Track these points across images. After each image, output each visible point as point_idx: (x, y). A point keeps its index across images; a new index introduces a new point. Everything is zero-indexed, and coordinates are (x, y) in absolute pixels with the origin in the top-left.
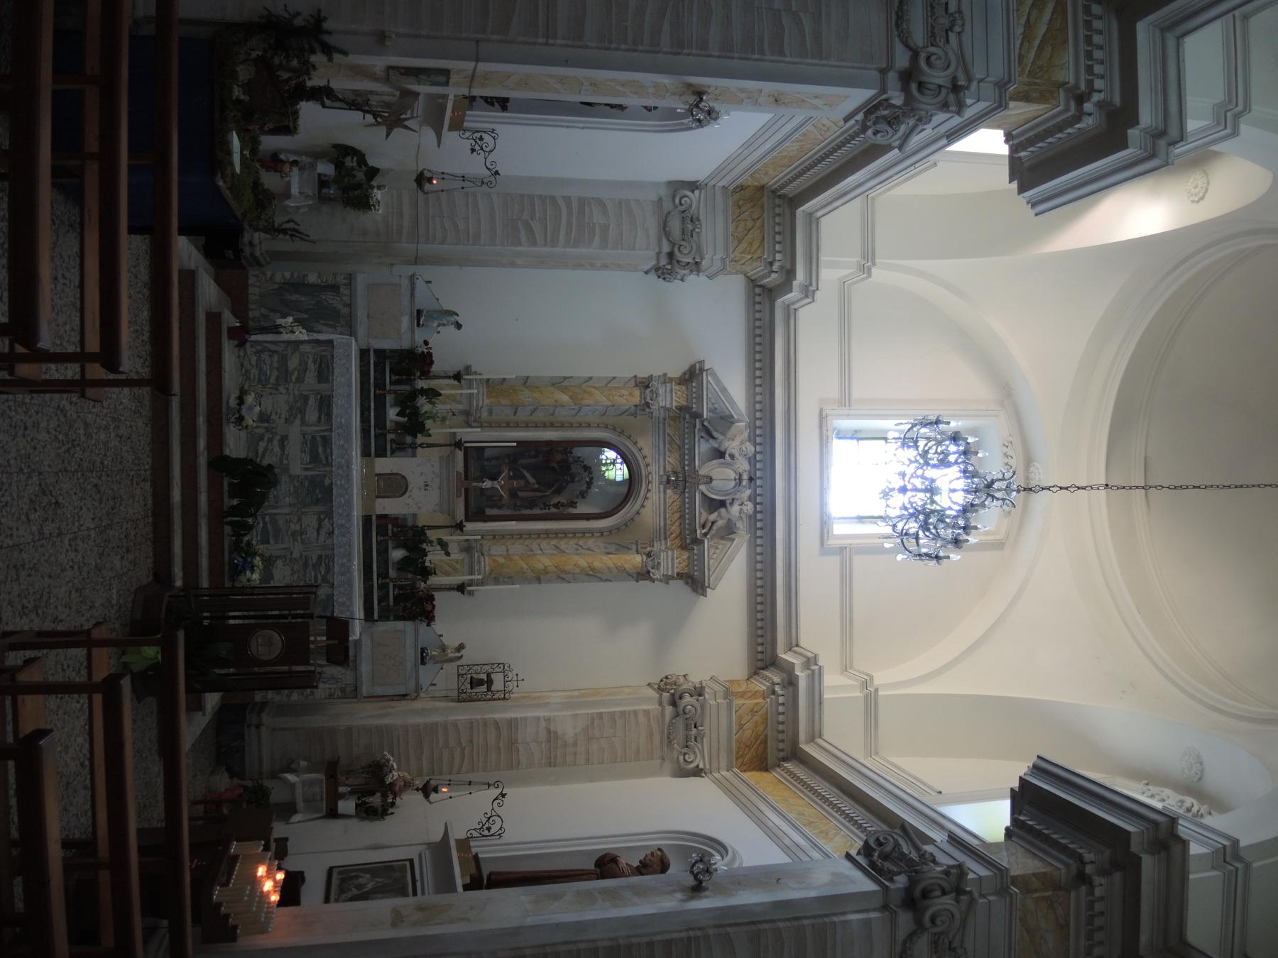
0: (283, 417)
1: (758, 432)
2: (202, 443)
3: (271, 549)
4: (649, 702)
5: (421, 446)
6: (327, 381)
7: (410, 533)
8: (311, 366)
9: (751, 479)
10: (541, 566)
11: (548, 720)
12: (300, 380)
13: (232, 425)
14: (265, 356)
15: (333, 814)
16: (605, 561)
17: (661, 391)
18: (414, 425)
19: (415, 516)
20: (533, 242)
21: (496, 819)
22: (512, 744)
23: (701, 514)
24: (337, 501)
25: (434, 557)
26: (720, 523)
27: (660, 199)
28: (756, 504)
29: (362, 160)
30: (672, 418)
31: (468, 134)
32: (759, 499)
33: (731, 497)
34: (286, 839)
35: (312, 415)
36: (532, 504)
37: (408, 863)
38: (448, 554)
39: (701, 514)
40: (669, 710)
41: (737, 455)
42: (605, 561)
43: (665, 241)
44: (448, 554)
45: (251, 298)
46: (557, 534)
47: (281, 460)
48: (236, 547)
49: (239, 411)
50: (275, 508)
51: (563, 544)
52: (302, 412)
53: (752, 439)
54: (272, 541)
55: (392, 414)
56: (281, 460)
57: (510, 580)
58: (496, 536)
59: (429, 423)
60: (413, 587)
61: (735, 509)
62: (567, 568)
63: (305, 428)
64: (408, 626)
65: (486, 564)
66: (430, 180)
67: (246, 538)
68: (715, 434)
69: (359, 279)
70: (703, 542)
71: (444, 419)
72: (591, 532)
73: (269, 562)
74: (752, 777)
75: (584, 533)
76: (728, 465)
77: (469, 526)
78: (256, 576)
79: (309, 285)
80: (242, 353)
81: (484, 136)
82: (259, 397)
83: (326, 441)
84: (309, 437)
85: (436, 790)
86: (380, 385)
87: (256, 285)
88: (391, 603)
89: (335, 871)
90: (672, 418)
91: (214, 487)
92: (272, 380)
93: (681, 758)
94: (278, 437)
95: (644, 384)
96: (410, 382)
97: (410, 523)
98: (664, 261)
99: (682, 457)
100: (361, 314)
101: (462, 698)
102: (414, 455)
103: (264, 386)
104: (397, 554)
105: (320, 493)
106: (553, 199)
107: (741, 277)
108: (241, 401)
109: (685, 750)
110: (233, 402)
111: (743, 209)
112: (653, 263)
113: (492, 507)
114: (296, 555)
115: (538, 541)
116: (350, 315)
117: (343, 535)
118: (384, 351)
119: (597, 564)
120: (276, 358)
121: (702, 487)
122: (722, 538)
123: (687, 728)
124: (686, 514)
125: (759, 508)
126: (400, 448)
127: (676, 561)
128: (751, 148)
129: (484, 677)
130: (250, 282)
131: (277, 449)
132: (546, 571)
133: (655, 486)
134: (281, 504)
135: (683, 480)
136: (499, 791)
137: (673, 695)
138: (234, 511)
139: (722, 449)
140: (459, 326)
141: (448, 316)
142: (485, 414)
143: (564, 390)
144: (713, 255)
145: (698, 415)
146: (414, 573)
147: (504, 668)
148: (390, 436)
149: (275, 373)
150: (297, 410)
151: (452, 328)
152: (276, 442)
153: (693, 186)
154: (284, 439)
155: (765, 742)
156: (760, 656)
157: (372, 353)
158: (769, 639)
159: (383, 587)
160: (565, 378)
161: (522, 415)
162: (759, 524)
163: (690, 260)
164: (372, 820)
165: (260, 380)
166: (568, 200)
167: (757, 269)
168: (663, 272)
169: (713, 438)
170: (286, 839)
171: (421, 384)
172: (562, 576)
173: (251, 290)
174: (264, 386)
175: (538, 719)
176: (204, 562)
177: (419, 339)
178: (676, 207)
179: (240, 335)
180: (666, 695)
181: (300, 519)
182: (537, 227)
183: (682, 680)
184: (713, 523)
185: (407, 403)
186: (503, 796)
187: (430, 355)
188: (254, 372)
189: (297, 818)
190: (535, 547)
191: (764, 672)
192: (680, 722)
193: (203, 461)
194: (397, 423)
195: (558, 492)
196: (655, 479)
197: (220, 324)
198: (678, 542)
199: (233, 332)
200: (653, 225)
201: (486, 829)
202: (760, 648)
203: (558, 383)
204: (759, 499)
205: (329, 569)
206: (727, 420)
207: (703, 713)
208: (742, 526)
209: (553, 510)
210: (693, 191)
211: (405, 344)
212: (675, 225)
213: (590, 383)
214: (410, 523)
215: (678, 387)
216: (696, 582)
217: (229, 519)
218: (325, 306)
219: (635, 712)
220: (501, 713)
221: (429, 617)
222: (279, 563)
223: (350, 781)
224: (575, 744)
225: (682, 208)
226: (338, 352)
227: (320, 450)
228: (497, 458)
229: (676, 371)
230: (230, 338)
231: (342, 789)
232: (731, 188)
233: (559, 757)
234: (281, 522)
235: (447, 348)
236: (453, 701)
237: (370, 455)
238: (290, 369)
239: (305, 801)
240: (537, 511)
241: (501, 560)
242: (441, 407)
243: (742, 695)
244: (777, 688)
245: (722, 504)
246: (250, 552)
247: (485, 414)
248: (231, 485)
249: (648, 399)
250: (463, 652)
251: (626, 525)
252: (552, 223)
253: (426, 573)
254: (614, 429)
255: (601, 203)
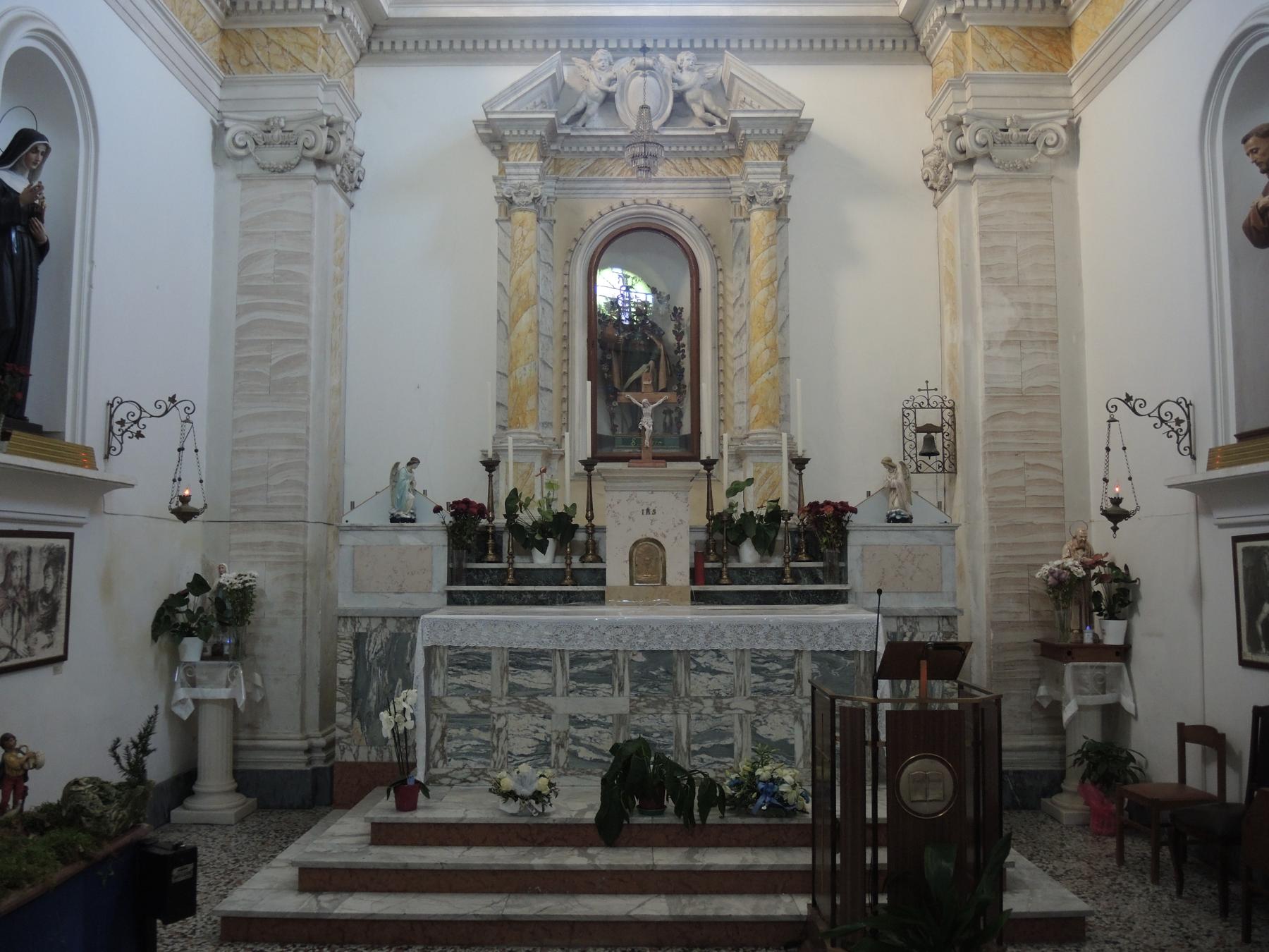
0: (541, 722)
1: (576, 45)
2: (573, 859)
3: (741, 740)
4: (966, 200)
5: (590, 518)
6: (488, 657)
7: (718, 536)
8: (463, 680)
9: (644, 50)
10: (766, 355)
11: (989, 344)
12: (486, 696)
13: (548, 809)
14: (450, 747)
15: (1123, 653)
16: (760, 264)
17: (516, 181)
18: (559, 527)
19: (693, 529)
20: (301, 359)
21: (1163, 410)
22: (1023, 396)
23: (694, 128)
24: (670, 643)
25: (752, 503)
26: (707, 100)
27: (239, 177)
28: (680, 49)
29: (180, 598)
30: (557, 169)
31: (115, 443)
32: (674, 45)
33: (670, 83)
34: (1181, 726)
35: (539, 679)
36: (675, 373)
37: (1240, 546)
38: (750, 481)
39: (694, 128)
40: (979, 168)
41: (610, 75)
42: (760, 264)
43: (299, 171)
44: (750, 481)
45: (374, 757)
46: (719, 334)
47: (608, 726)
48: (741, 805)
49: (524, 798)
50: (678, 739)
51: (734, 326)
52: (534, 694)
53: (587, 54)
54: (728, 741)
55: (543, 560)
56: (608, 726)
57: (783, 399)
58: (721, 421)
59: (558, 508)
60: (797, 533)
61: (687, 78)
62: (768, 317)
63: (559, 690)
64: (855, 543)
65: (762, 432)
66: (185, 500)
67: (728, 791)
68: (579, 107)
69: (346, 606)
70: (735, 120)
71: (551, 485)
72: (718, 284)
73: (767, 749)
74: (1080, 47)
75: (719, 296)
76: (624, 87)
77: (707, 451)
78: (788, 775)
79: (355, 676)
80: (446, 781)
81: (117, 418)
82: (512, 761)
83: (579, 658)
84: (573, 685)
85: (1117, 501)
86: (500, 577)
87: (355, 752)
88: (821, 564)
89: (1248, 656)
90: (557, 169)
91: (647, 839)
92: (486, 736)
93: (1051, 151)
94: (572, 729)
95: (508, 204)
96: (497, 535)
97: (702, 536)
98: (329, 174)
99: (615, 156)
100: (396, 603)
101: (950, 468)
102: (603, 529)
103: (495, 749)
104: (749, 555)
105: (657, 670)
106: (241, 331)
107: (357, 71)
108: (510, 795)
109: (1040, 146)
110: (513, 807)
111: (254, 59)
112: (332, 190)
113: (680, 424)
114: (750, 706)
115: (729, 360)
116: (398, 618)
117: (723, 635)
118: (450, 571)
119: (764, 274)
120: (452, 732)
121: (656, 125)
122: (728, 99)
123: (1006, 142)
124: (692, 152)
125: (686, 45)
126: (593, 550)
127: (761, 161)
128: (138, 17)
129: (921, 436)
130: (351, 759)
131: (591, 731)
132: (773, 348)
133: (654, 196)
134: (672, 728)
135: (645, 152)
136: (1121, 405)
137: (955, 165)
138: (683, 809)
139: (601, 96)
140: (414, 462)
141: (401, 475)
142: (550, 433)
143: (515, 320)
144: (324, 101)
145: (552, 127)
146: (777, 530)
147: (910, 407)
148: (576, 563)
149: (475, 732)
150: (531, 701)
151: (418, 472)
152: (580, 733)
153: (219, 131)
154: (575, 721)
155: (1029, 30)
156: (900, 46)
157: (453, 588)
158: (873, 31)
159: (796, 577)
160: (500, 320)
161: (550, 380)
162: (710, 45)
163: (325, 133)
164: (1137, 596)
165: (488, 755)
166: (242, 310)
167: (343, 45)
168: (350, 184)
169: (585, 109)
170: (1181, 726)
171: (500, 521)
172: (779, 325)
173: (363, 758)
174: (495, 749)
175: (988, 359)
176: (766, 859)
177: (435, 520)
178: (249, 154)
179: (407, 795)
180: (956, 174)
181: (697, 699)
182: (278, 355)
183: (930, 158)
184: (707, 110)
185: (528, 539)
186: (1129, 398)
187: (456, 504)
188: (474, 763)
189: (1128, 703)
190: (736, 365)
191: (924, 37)
192: (999, 153)
193: (605, 858)
194: (557, 553)
195: (660, 335)
196: (641, 195)
197: (392, 825)
198: (733, 162)
199: (406, 801)
200: (278, 188)
201: (1180, 425)
202: (888, 45)
203: (506, 326)
204: (674, 45)
205: (773, 658)
206: (558, 90)
207: (990, 119)
208: (712, 70)
209: (685, 340)
210: (226, 129)
211: (441, 539)
212: (277, 156)
213: (506, 284)
214: (702, 536)
215: (511, 157)
216: (791, 134)
217: (696, 814)
218: (379, 656)
219: (982, 218)
220: (975, 414)
221: (842, 510)
222: (762, 731)
223: (1074, 626)
224: (1026, 305)
225: (251, 145)
226: (443, 639)
227: (591, 667)
228: (612, 416)
229: (491, 164)
230: (413, 807)
231: (1088, 639)
232: (221, 74)
233: (1044, 330)
234: (702, 727)
235: (450, 478)
236: (952, 481)
237: (603, 593)
238: (469, 710)
239: (1103, 689)
240: (686, 364)
241: (756, 410)
242: (536, 491)
243: (959, 64)
244: (952, 10)
245: (679, 98)
246: (749, 784)
247: (550, 433)
248: (643, 811)
249: (529, 199)
250: (896, 461)
251: (708, 236)
252: (275, 334)
253: (776, 514)
254: (571, 251)
255: (245, 263)
